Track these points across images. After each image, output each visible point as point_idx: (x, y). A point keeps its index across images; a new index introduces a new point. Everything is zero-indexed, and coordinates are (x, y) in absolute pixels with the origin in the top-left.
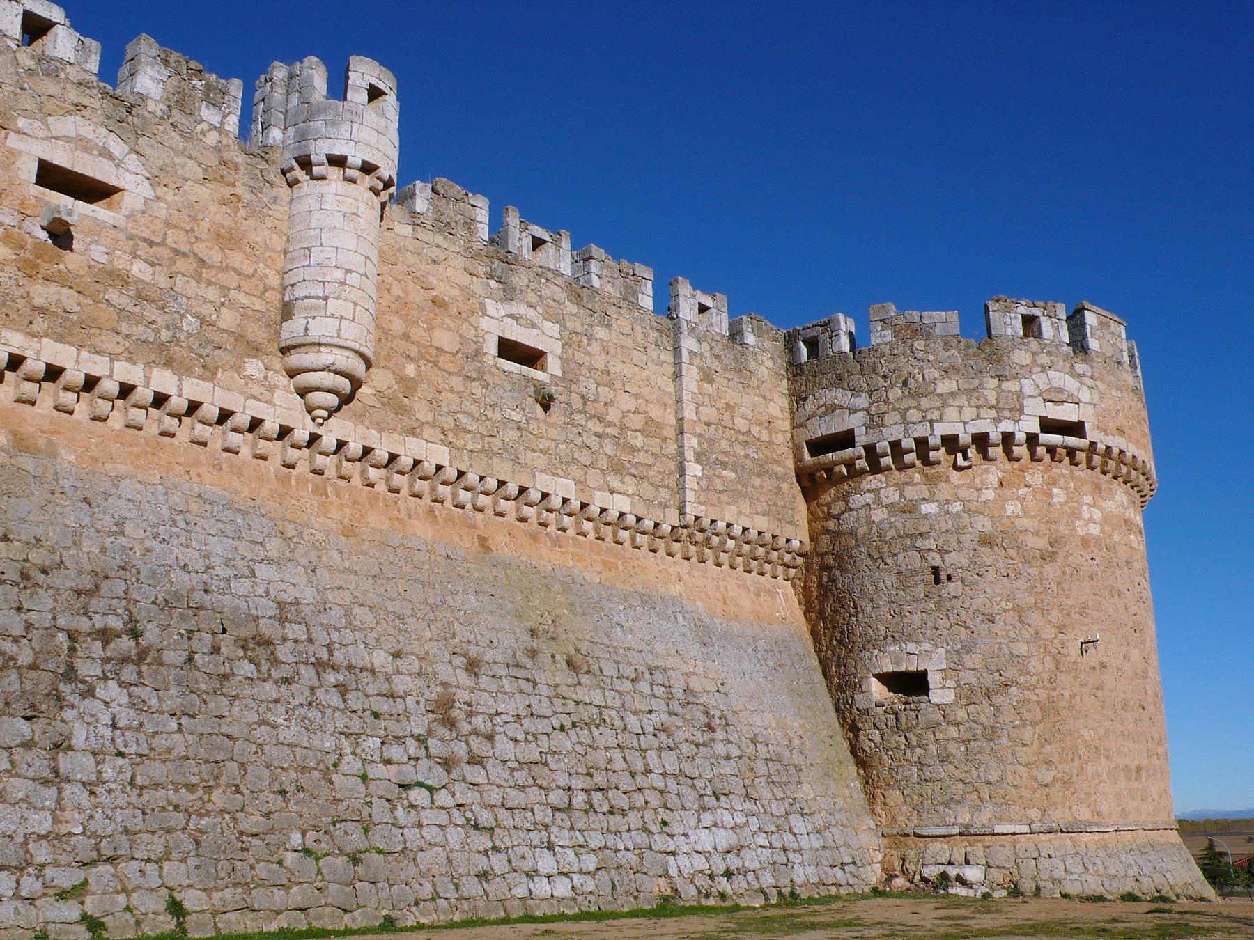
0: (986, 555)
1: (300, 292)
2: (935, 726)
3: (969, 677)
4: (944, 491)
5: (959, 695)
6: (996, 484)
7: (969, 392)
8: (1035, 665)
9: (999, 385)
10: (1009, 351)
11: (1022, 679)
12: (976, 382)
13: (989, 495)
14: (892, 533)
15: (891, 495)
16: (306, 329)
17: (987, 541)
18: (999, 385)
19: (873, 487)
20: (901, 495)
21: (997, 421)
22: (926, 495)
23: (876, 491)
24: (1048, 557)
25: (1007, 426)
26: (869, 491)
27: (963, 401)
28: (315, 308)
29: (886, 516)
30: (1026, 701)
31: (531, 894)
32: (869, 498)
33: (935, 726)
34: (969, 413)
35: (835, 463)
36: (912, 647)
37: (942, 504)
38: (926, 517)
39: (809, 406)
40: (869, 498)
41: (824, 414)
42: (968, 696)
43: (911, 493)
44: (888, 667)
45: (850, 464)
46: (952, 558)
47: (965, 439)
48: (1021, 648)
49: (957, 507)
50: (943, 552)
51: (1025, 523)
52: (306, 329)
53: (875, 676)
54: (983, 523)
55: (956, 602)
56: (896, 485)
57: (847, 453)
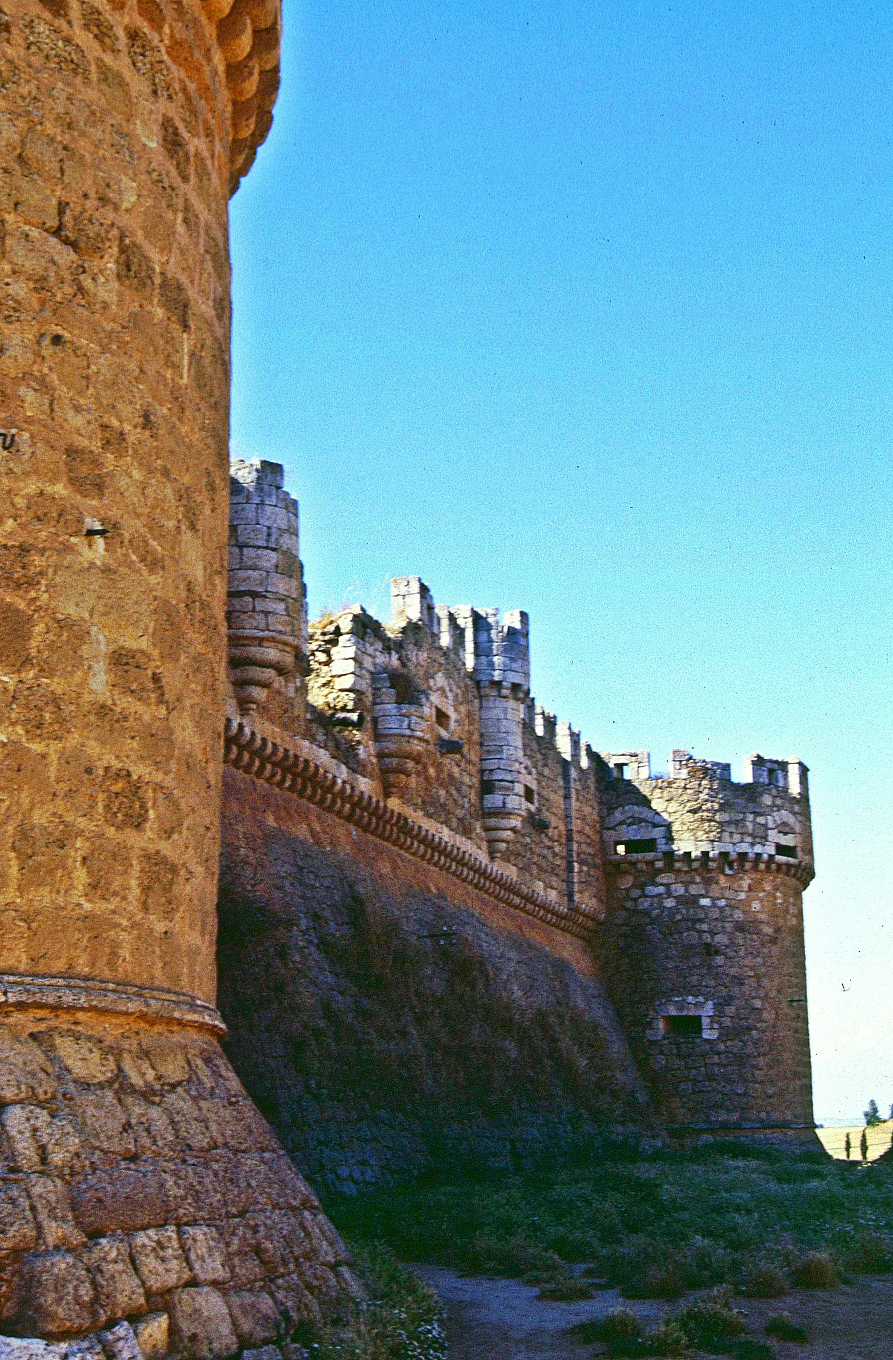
0: (740, 938)
1: (498, 776)
2: (704, 1055)
3: (727, 1022)
4: (715, 890)
5: (721, 1034)
6: (746, 889)
7: (737, 823)
8: (765, 1015)
9: (754, 819)
10: (761, 795)
11: (758, 1025)
12: (741, 816)
13: (742, 896)
14: (679, 917)
15: (679, 889)
16: (504, 803)
17: (740, 927)
18: (754, 819)
19: (665, 881)
20: (686, 891)
21: (752, 845)
22: (703, 892)
23: (667, 886)
24: (773, 941)
25: (758, 849)
26: (661, 884)
27: (732, 828)
28: (508, 789)
29: (674, 904)
30: (760, 1039)
31: (44, 1160)
32: (662, 889)
33: (704, 1055)
34: (737, 837)
35: (638, 861)
36: (690, 999)
37: (714, 899)
38: (703, 907)
39: (618, 815)
40: (662, 889)
41: (632, 824)
42: (726, 1034)
43: (693, 890)
44: (673, 1011)
45: (651, 863)
46: (718, 938)
47: (733, 856)
48: (758, 1003)
49: (722, 903)
50: (713, 933)
51: (762, 917)
52: (504, 803)
53: (663, 1017)
54: (738, 915)
55: (721, 970)
56: (682, 882)
57: (650, 856)
